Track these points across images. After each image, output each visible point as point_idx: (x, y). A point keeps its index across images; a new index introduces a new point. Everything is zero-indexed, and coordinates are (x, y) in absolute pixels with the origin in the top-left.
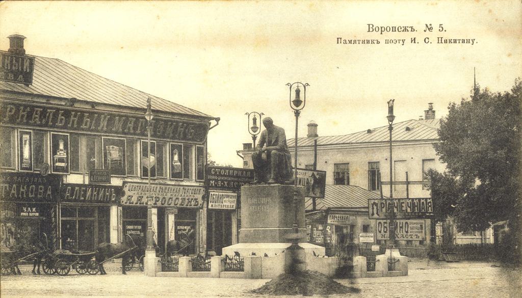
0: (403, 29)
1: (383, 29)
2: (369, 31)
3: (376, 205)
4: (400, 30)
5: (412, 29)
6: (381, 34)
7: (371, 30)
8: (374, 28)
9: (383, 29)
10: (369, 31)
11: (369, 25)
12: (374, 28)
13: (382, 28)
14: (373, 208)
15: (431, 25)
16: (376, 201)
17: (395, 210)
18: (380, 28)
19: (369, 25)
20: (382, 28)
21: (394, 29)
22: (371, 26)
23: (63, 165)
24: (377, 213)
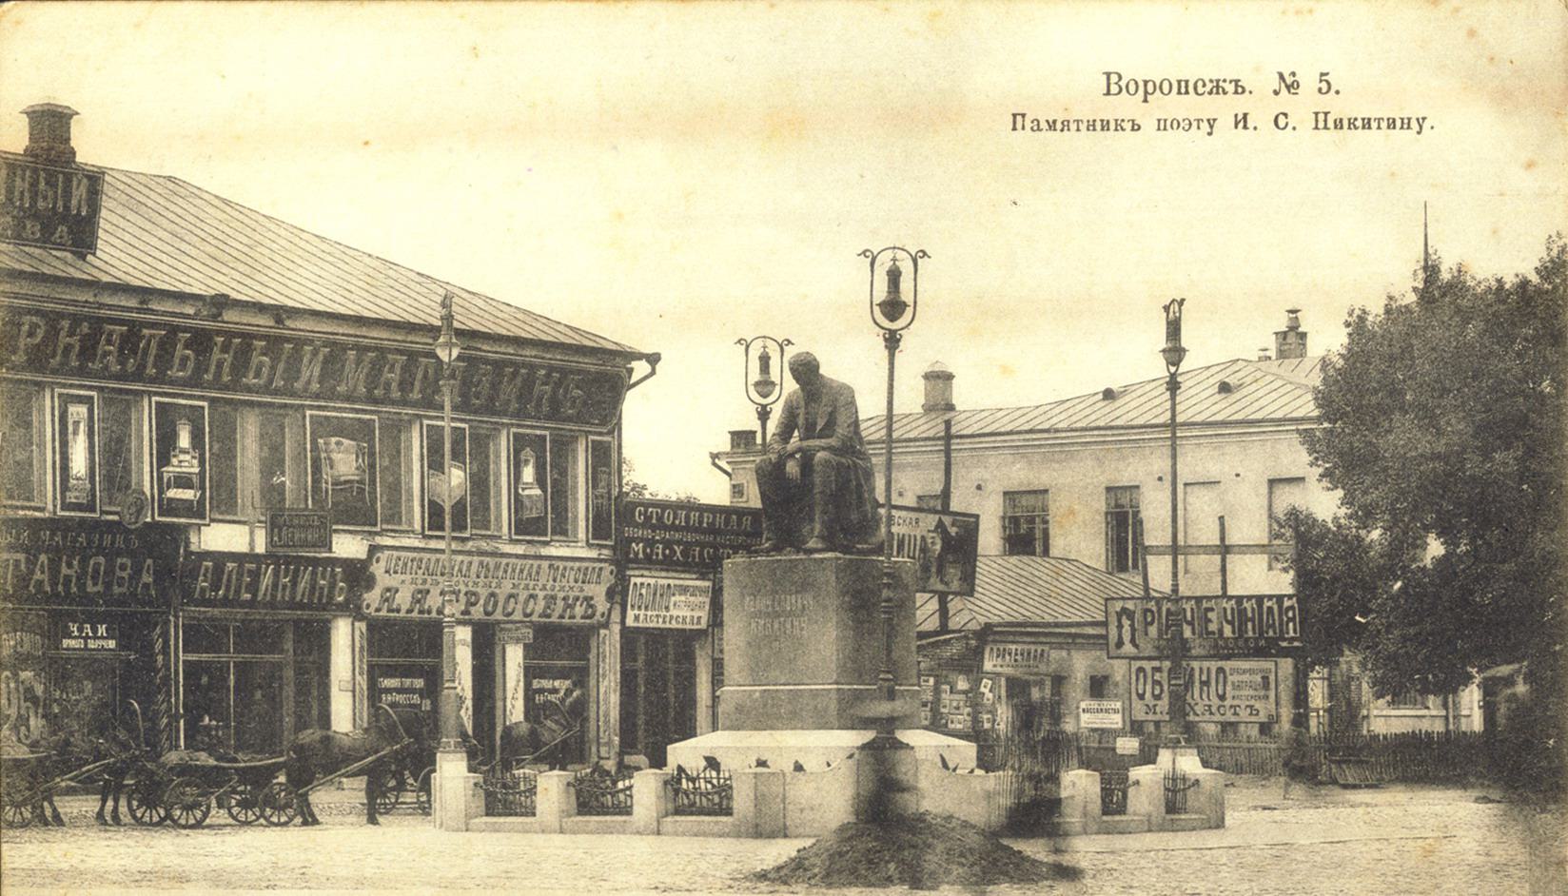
0: (1209, 86)
1: (1150, 88)
2: (1108, 93)
3: (1130, 615)
4: (1200, 90)
6: (1145, 101)
7: (1114, 89)
8: (1123, 84)
9: (1150, 88)
10: (1108, 93)
11: (1108, 75)
12: (1123, 84)
13: (1146, 83)
14: (1120, 626)
15: (1293, 74)
16: (1130, 605)
17: (1187, 633)
19: (1108, 75)
20: (1146, 83)
21: (1183, 87)
22: (1114, 78)
23: (188, 494)
24: (1133, 641)
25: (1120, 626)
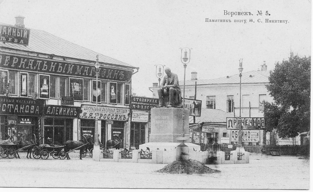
0: (244, 13)
5: (250, 13)
9: (233, 14)
12: (227, 13)
14: (229, 123)
16: (231, 119)
18: (231, 13)
20: (232, 13)
22: (226, 11)
25: (229, 123)
